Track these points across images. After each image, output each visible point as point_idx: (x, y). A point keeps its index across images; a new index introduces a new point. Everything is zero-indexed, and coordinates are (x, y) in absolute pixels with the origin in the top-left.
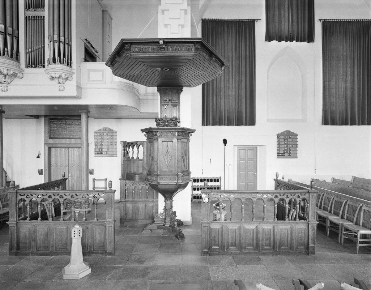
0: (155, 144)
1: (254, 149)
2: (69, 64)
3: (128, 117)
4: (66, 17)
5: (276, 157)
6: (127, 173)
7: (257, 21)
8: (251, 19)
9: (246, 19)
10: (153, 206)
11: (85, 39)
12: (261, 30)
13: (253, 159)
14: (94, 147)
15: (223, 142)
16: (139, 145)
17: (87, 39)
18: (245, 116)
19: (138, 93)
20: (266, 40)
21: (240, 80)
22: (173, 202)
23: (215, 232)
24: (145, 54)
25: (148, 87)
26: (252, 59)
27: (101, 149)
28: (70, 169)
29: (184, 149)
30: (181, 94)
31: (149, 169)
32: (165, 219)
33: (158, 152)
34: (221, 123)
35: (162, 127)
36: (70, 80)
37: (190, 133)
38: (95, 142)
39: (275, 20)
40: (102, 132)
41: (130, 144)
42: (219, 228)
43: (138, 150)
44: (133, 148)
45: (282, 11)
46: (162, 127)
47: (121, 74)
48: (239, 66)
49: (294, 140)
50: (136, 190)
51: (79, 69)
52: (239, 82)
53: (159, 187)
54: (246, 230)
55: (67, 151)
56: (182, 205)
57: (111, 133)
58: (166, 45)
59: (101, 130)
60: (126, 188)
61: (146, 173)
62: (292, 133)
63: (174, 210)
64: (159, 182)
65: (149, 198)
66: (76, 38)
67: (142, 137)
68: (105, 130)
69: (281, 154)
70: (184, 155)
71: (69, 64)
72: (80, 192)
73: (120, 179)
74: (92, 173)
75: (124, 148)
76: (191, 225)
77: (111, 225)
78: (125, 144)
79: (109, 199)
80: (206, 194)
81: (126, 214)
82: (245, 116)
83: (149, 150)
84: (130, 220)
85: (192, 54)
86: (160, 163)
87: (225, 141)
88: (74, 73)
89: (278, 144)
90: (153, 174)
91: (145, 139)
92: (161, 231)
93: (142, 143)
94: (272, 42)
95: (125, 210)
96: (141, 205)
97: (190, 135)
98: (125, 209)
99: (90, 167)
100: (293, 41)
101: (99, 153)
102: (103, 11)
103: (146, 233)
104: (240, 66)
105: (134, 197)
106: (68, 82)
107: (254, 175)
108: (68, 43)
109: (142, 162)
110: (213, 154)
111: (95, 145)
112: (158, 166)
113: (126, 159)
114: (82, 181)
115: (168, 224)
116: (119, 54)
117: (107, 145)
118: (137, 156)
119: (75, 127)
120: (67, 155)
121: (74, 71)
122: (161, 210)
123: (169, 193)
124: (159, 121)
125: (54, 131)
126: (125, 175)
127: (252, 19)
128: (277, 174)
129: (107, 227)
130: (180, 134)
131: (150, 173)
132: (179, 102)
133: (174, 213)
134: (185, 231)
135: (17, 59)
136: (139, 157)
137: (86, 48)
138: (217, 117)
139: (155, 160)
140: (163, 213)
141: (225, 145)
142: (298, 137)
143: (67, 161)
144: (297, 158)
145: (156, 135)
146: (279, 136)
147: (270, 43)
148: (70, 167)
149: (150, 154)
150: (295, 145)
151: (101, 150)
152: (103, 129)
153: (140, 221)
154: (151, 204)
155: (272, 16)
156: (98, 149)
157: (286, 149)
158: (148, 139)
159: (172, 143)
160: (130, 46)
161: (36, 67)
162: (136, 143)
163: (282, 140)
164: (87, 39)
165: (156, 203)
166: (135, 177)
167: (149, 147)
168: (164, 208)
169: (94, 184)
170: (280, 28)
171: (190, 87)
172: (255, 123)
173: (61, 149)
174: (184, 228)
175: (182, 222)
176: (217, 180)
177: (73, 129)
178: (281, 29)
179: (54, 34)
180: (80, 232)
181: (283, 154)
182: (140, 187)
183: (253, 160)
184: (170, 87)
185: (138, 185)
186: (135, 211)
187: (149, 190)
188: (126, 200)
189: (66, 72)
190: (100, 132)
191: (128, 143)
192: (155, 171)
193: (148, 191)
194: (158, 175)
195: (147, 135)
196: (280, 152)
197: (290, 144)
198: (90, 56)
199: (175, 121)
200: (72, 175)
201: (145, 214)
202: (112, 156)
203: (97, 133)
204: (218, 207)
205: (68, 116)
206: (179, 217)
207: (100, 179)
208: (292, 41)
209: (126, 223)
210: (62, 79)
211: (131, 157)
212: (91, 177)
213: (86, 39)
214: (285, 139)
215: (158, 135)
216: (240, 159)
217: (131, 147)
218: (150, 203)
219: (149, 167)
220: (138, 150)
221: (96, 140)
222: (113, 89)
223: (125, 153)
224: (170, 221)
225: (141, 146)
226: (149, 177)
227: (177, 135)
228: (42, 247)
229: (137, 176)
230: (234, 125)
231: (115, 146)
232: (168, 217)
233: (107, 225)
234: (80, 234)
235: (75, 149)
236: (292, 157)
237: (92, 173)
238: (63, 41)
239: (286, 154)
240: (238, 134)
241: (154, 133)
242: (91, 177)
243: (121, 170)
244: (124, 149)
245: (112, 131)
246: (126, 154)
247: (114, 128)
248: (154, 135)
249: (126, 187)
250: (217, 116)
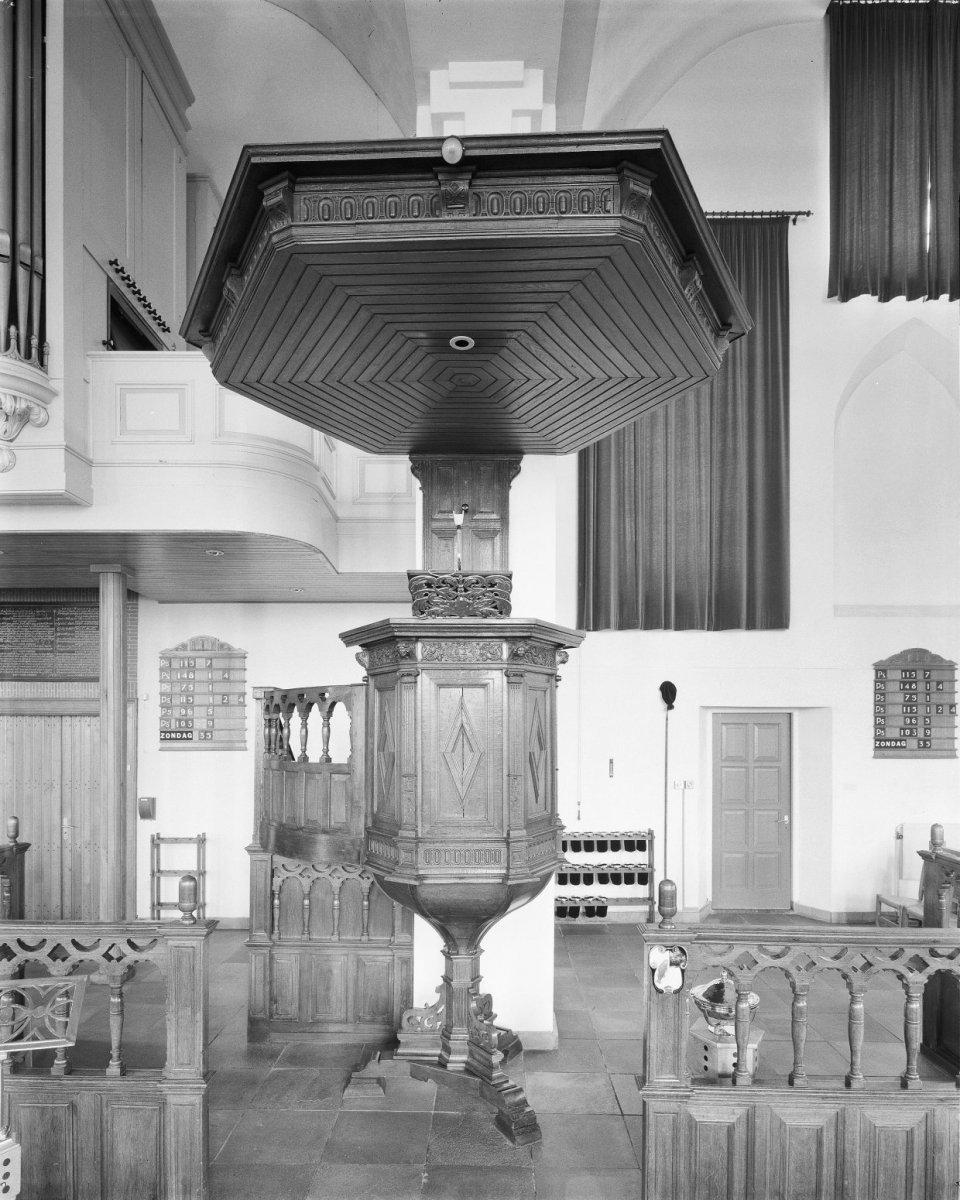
0: (407, 696)
1: (781, 722)
2: (34, 352)
3: (290, 597)
5: (872, 753)
6: (281, 825)
7: (794, 221)
8: (770, 213)
9: (753, 214)
10: (391, 966)
11: (111, 263)
12: (810, 252)
13: (771, 759)
14: (158, 712)
15: (659, 694)
16: (333, 704)
17: (115, 262)
18: (748, 591)
19: (331, 491)
20: (830, 295)
21: (730, 452)
22: (483, 958)
23: (711, 1141)
24: (365, 233)
26: (777, 368)
27: (187, 722)
28: (67, 798)
29: (536, 724)
30: (514, 483)
31: (375, 809)
32: (446, 1033)
33: (419, 732)
34: (653, 621)
35: (439, 620)
36: (40, 426)
37: (560, 646)
38: (162, 694)
39: (867, 214)
40: (192, 654)
41: (293, 698)
42: (733, 1119)
43: (327, 725)
45: (896, 179)
46: (439, 620)
47: (253, 376)
48: (724, 397)
49: (940, 687)
50: (319, 893)
51: (80, 384)
52: (725, 458)
53: (425, 893)
54: (872, 1135)
56: (519, 968)
57: (227, 659)
58: (470, 185)
59: (184, 647)
60: (276, 888)
61: (362, 826)
62: (936, 658)
63: (484, 988)
64: (421, 872)
65: (371, 930)
66: (67, 243)
67: (347, 668)
68: (200, 647)
69: (890, 740)
70: (536, 749)
71: (34, 352)
72: (41, 932)
73: (250, 850)
74: (148, 812)
75: (267, 717)
76: (555, 1051)
77: (193, 1098)
79: (178, 968)
80: (671, 949)
81: (273, 1000)
82: (748, 591)
83: (376, 724)
84: (290, 1025)
85: (604, 224)
86: (426, 782)
87: (668, 692)
88: (54, 394)
89: (877, 703)
90: (396, 835)
91: (358, 674)
92: (430, 1087)
93: (345, 694)
94: (854, 301)
95: (271, 983)
96: (340, 963)
97: (558, 658)
98: (271, 975)
99: (144, 792)
100: (937, 298)
101: (176, 734)
102: (191, 179)
103: (360, 1098)
104: (730, 397)
105: (307, 928)
106: (28, 434)
107: (779, 821)
108: (28, 262)
109: (343, 778)
110: (633, 738)
111: (162, 706)
112: (420, 798)
113: (275, 764)
114: (102, 851)
115: (458, 1061)
116: (234, 260)
117: (208, 706)
119: (80, 639)
120: (56, 741)
121: (58, 384)
122: (426, 987)
123: (465, 922)
124: (429, 585)
126: (272, 833)
127: (777, 213)
128: (938, 830)
129: (171, 1110)
130: (521, 651)
131: (383, 828)
132: (504, 519)
133: (487, 1002)
134: (541, 1090)
137: (112, 297)
138: (637, 596)
139: (405, 770)
140: (435, 1007)
141: (670, 707)
143: (56, 766)
144: (955, 757)
145: (411, 655)
146: (881, 670)
147: (845, 304)
148: (67, 791)
149: (382, 745)
150: (946, 708)
151: (183, 724)
152: (194, 642)
153: (333, 1028)
154: (381, 958)
155: (856, 197)
156: (173, 721)
157: (911, 723)
158: (372, 674)
159: (481, 691)
160: (290, 191)
162: (321, 693)
163: (894, 687)
164: (115, 262)
165: (405, 954)
166: (311, 842)
167: (377, 711)
168: (441, 982)
169: (156, 859)
170: (887, 248)
171: (552, 452)
172: (788, 619)
173: (36, 720)
174: (529, 1070)
175: (516, 1037)
176: (636, 845)
177: (79, 643)
178: (891, 249)
180: (7, 1169)
181: (901, 741)
182: (336, 883)
183: (775, 764)
184: (465, 453)
185: (325, 877)
186: (314, 988)
187: (373, 898)
188: (275, 937)
189: (20, 385)
190: (181, 653)
191: (285, 696)
192: (405, 819)
193: (369, 900)
194: (418, 840)
195: (366, 659)
196: (888, 736)
197: (928, 704)
198: (129, 330)
199: (496, 591)
200: (72, 820)
201: (355, 1001)
202: (229, 746)
203: (170, 660)
204: (721, 1010)
205: (68, 591)
206: (506, 1017)
207: (181, 836)
208: (934, 295)
209: (279, 1041)
211: (297, 753)
212: (145, 829)
213: (114, 263)
214: (907, 682)
215: (419, 656)
216: (724, 761)
218: (378, 952)
219: (375, 804)
220: (327, 725)
221: (166, 688)
222: (220, 464)
223: (270, 736)
224: (470, 1042)
225: (340, 707)
226: (374, 846)
227: (505, 655)
229: (322, 838)
230: (703, 628)
231: (237, 710)
232: (461, 1026)
233: (172, 1100)
234: (9, 1182)
235: (88, 719)
236: (934, 753)
237: (148, 812)
239: (913, 743)
240: (717, 664)
241: (402, 647)
242: (145, 829)
243: (255, 810)
244: (270, 720)
245: (229, 649)
246: (276, 743)
247: (236, 640)
248: (403, 658)
249: (277, 881)
250: (637, 592)
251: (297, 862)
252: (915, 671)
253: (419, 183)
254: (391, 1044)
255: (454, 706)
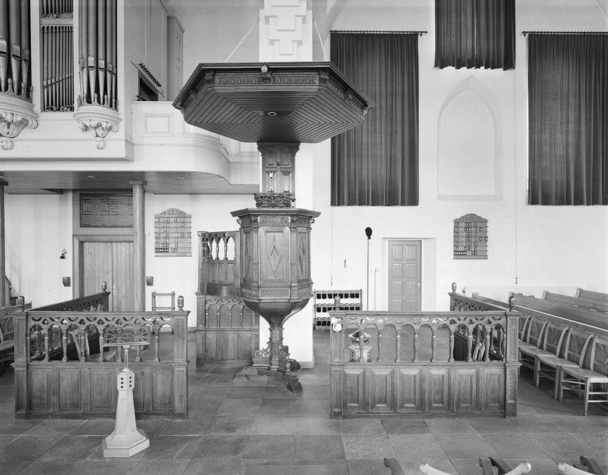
0: (255, 235)
1: (417, 244)
2: (113, 104)
3: (210, 192)
4: (108, 28)
5: (453, 257)
6: (209, 283)
7: (421, 35)
8: (411, 32)
9: (403, 32)
10: (251, 338)
11: (140, 65)
12: (427, 48)
13: (414, 260)
14: (154, 241)
15: (365, 232)
16: (228, 238)
17: (142, 64)
18: (402, 191)
19: (227, 152)
20: (436, 66)
21: (394, 132)
22: (284, 332)
23: (352, 380)
24: (238, 89)
25: (242, 143)
26: (413, 97)
27: (166, 244)
28: (115, 277)
29: (302, 244)
30: (297, 154)
31: (244, 277)
32: (271, 358)
33: (259, 248)
34: (363, 202)
35: (266, 209)
36: (115, 132)
37: (311, 217)
38: (156, 233)
39: (451, 33)
40: (168, 216)
41: (213, 236)
42: (359, 373)
43: (226, 246)
44: (218, 242)
45: (462, 19)
46: (266, 209)
47: (199, 121)
48: (392, 109)
49: (481, 229)
50: (223, 311)
51: (129, 113)
52: (392, 134)
53: (261, 306)
54: (403, 377)
55: (110, 248)
56: (298, 336)
57: (183, 218)
58: (271, 74)
59: (165, 213)
60: (207, 308)
61: (239, 283)
62: (479, 217)
63: (285, 343)
64: (260, 298)
65: (243, 324)
66: (125, 62)
67: (233, 225)
68: (172, 213)
69: (460, 252)
70: (302, 255)
71: (113, 104)
72: (132, 315)
73: (197, 294)
74: (150, 283)
75: (203, 243)
76: (313, 368)
77: (183, 368)
78: (205, 235)
79: (178, 326)
80: (338, 318)
81: (206, 351)
82: (402, 190)
83: (244, 246)
85: (314, 88)
86: (262, 267)
87: (369, 232)
88: (121, 120)
89: (455, 237)
91: (237, 227)
92: (264, 378)
93: (233, 234)
94: (445, 69)
95: (205, 345)
96: (231, 337)
97: (311, 221)
98: (205, 342)
99: (148, 274)
100: (479, 68)
101: (162, 250)
102: (169, 18)
103: (239, 381)
104: (394, 108)
105: (219, 323)
106: (111, 135)
107: (416, 286)
108: (111, 70)
109: (232, 265)
110: (349, 252)
111: (156, 238)
112: (259, 272)
113: (206, 261)
114: (135, 297)
115: (275, 368)
116: (194, 88)
117: (175, 238)
118: (224, 256)
119: (122, 209)
120: (110, 253)
121: (122, 116)
122: (264, 344)
123: (277, 317)
124: (261, 197)
125: (88, 215)
126: (205, 287)
127: (413, 32)
128: (454, 285)
129: (176, 373)
130: (295, 219)
131: (246, 283)
132: (293, 167)
133: (286, 349)
135: (28, 97)
136: (227, 256)
137: (140, 78)
138: (356, 192)
139: (254, 262)
140: (267, 349)
141: (369, 238)
142: (488, 224)
143: (110, 263)
144: (487, 259)
145: (256, 221)
146: (457, 222)
147: (442, 70)
148: (114, 273)
149: (245, 252)
150: (484, 238)
151: (165, 245)
152: (169, 211)
153: (229, 361)
154: (247, 335)
155: (446, 26)
157: (469, 245)
158: (243, 227)
159: (281, 234)
160: (214, 76)
161: (59, 110)
162: (224, 234)
163: (462, 230)
164: (142, 64)
165: (256, 333)
166: (221, 289)
167: (244, 240)
168: (268, 340)
169: (154, 302)
170: (459, 47)
171: (311, 142)
172: (418, 201)
173: (101, 244)
174: (302, 374)
175: (298, 363)
176: (355, 295)
177: (120, 211)
178: (461, 47)
179: (88, 55)
180: (131, 380)
181: (465, 252)
182: (230, 306)
183: (414, 262)
184: (279, 142)
185: (226, 304)
186: (222, 346)
187: (244, 312)
188: (207, 327)
189: (109, 118)
190: (163, 216)
191: (210, 235)
192: (254, 279)
193: (242, 313)
194: (259, 287)
195: (240, 222)
196: (460, 250)
197: (476, 237)
199: (287, 199)
200: (117, 286)
201: (237, 351)
202: (184, 255)
203: (159, 218)
204: (358, 339)
205: (111, 190)
206: (293, 355)
207: (164, 292)
208: (478, 67)
209: (207, 366)
210: (101, 130)
211: (214, 257)
212: (149, 290)
213: (141, 65)
214: (467, 228)
215: (259, 221)
217: (214, 241)
219: (244, 274)
220: (226, 246)
221: (158, 230)
222: (184, 145)
223: (204, 251)
224: (279, 361)
225: (231, 239)
226: (244, 290)
227: (290, 221)
228: (69, 404)
229: (225, 288)
230: (383, 205)
231: (188, 240)
232: (276, 355)
233: (176, 369)
234: (131, 384)
235: (123, 243)
236: (478, 257)
237: (150, 283)
238: (103, 66)
239: (469, 253)
240: (389, 220)
241: (253, 218)
242: (149, 290)
243: (199, 279)
244: (204, 244)
245: (184, 214)
246: (206, 252)
247: (187, 210)
248: (253, 222)
249: (207, 306)
250: (356, 189)
251: (215, 297)
252: (471, 223)
253: (255, 74)
254: (251, 364)
255: (272, 240)
